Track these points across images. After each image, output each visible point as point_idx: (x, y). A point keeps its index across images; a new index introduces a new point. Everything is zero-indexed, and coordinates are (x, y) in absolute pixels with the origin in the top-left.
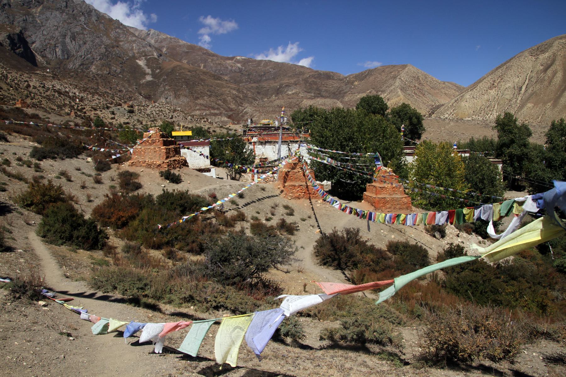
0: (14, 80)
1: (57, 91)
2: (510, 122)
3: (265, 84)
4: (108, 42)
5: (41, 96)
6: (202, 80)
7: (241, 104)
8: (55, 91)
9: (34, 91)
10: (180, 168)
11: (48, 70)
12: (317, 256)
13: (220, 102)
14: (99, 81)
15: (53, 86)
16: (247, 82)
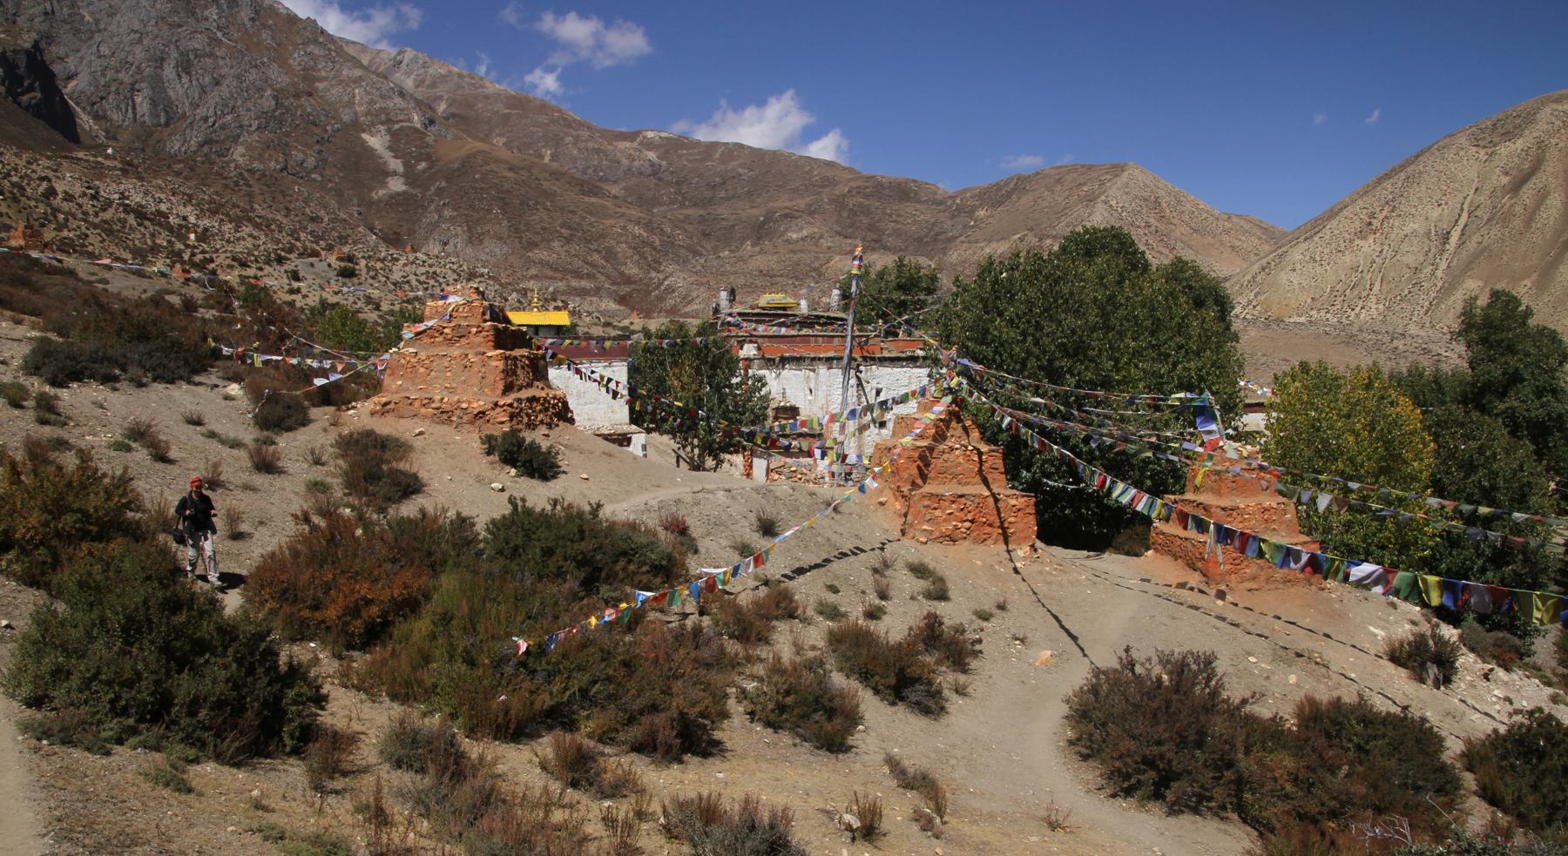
0: (8, 175)
1: (134, 211)
2: (1508, 317)
3: (723, 211)
4: (284, 80)
5: (85, 221)
7: (655, 265)
8: (127, 209)
9: (66, 206)
10: (550, 426)
11: (110, 151)
12: (1085, 758)
13: (596, 256)
14: (256, 189)
15: (123, 196)
16: (672, 202)
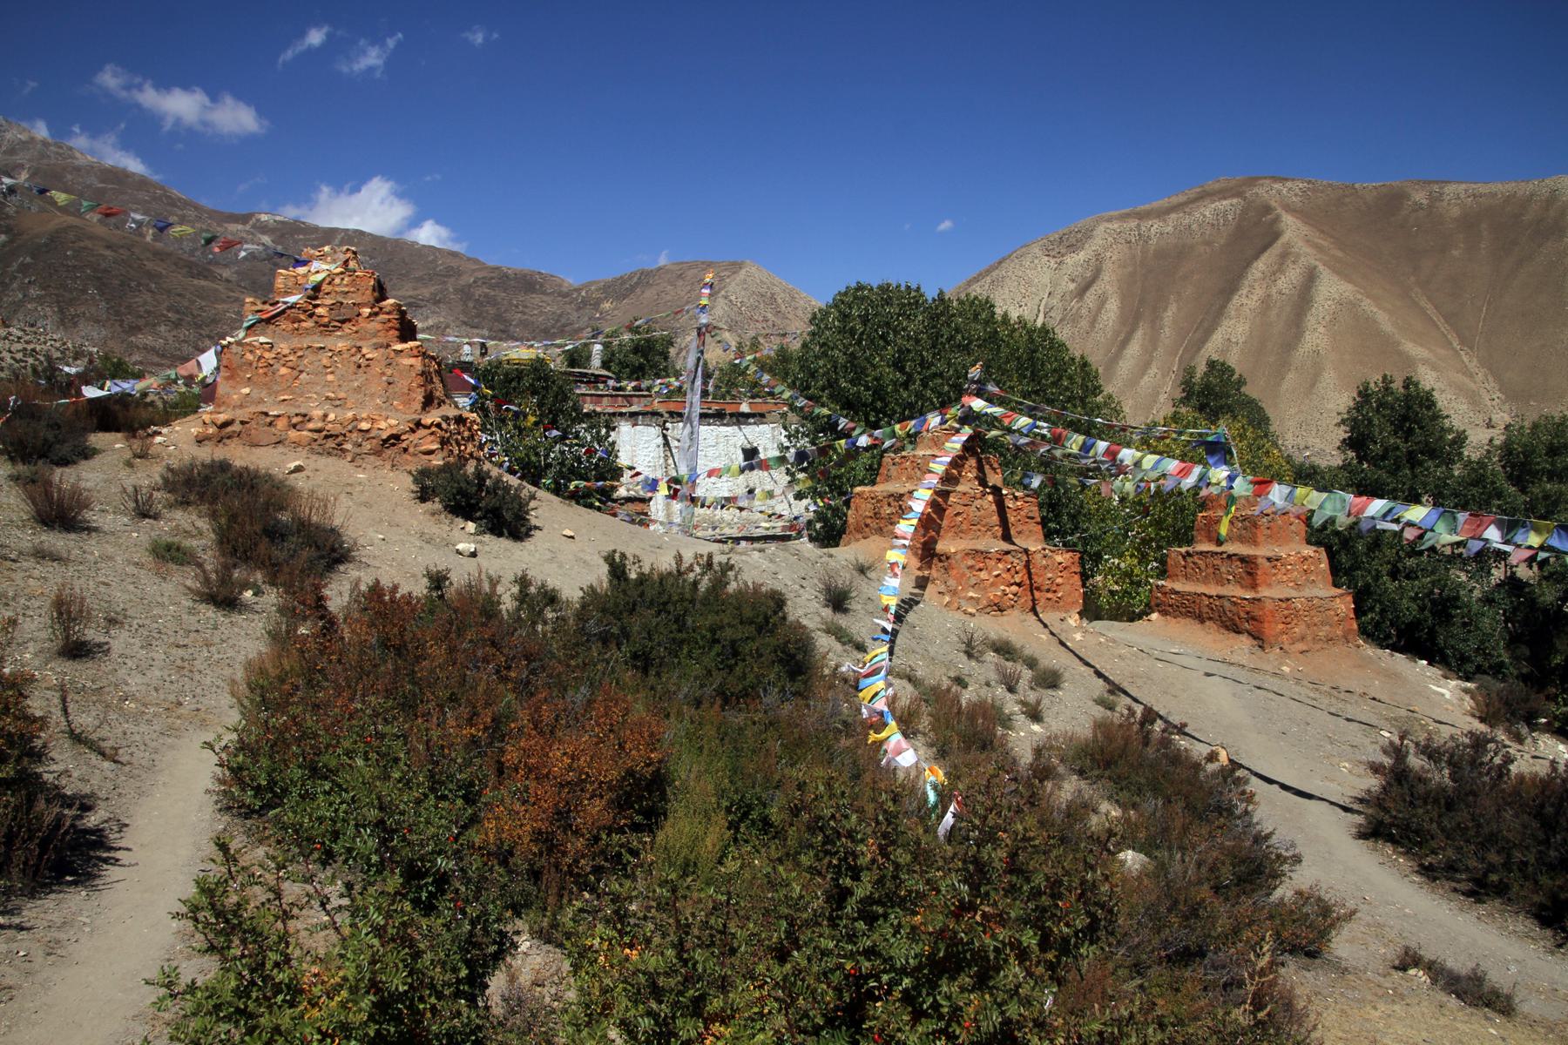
6: (151, 276)
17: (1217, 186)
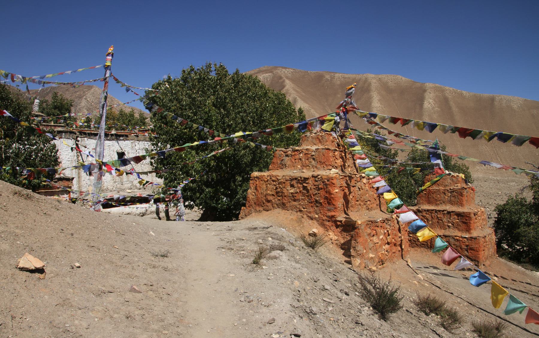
17: (264, 69)
